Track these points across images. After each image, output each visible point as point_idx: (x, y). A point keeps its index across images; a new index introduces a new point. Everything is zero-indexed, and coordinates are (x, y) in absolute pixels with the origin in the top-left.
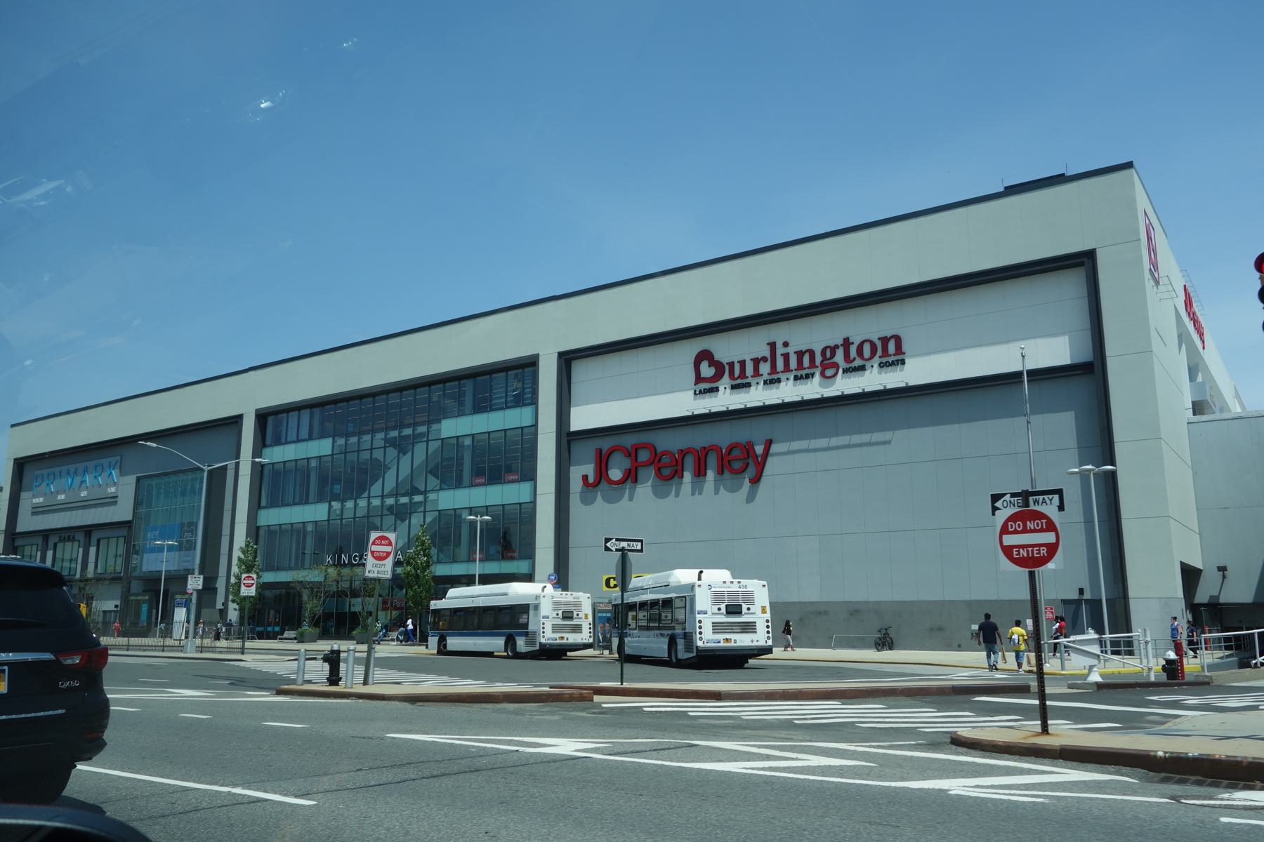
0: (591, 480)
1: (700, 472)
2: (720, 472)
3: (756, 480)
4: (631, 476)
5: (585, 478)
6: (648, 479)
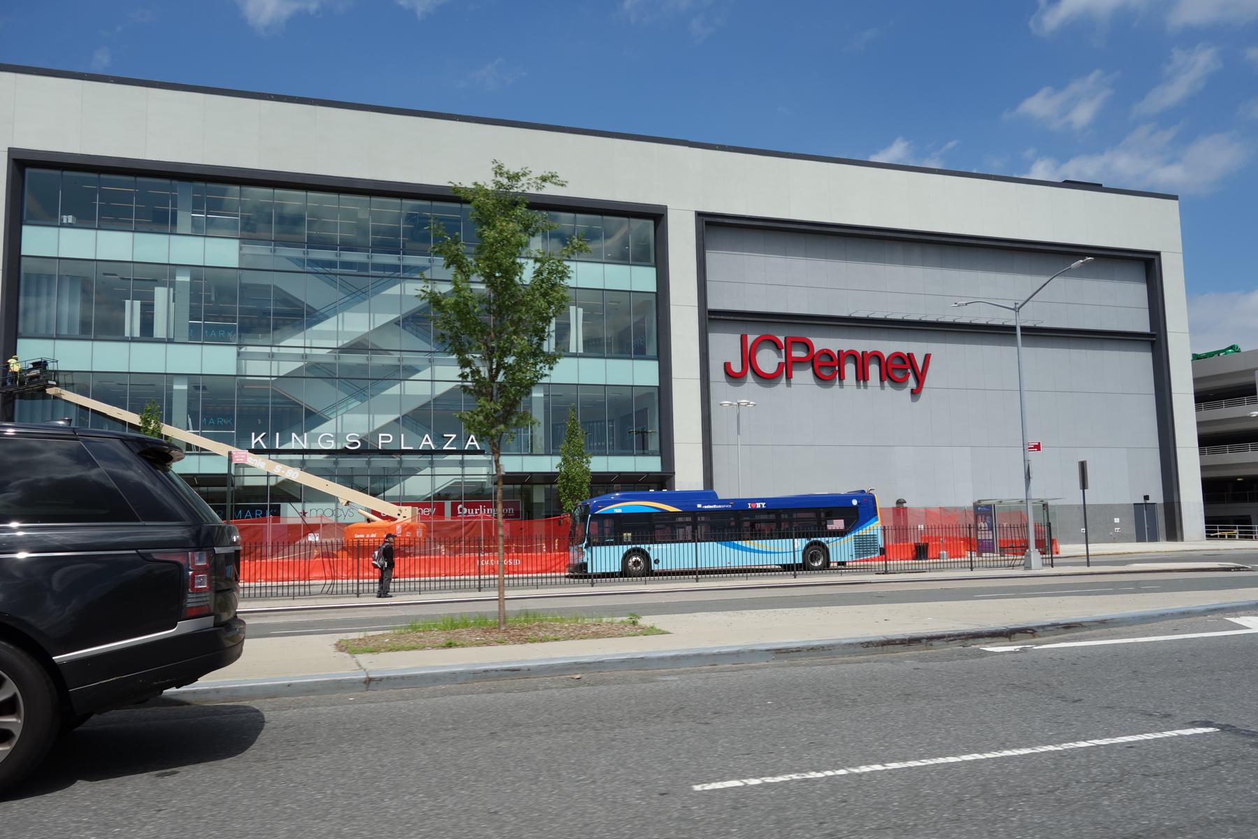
0: (736, 368)
1: (862, 376)
2: (882, 380)
3: (915, 393)
4: (786, 369)
5: (727, 366)
6: (804, 376)
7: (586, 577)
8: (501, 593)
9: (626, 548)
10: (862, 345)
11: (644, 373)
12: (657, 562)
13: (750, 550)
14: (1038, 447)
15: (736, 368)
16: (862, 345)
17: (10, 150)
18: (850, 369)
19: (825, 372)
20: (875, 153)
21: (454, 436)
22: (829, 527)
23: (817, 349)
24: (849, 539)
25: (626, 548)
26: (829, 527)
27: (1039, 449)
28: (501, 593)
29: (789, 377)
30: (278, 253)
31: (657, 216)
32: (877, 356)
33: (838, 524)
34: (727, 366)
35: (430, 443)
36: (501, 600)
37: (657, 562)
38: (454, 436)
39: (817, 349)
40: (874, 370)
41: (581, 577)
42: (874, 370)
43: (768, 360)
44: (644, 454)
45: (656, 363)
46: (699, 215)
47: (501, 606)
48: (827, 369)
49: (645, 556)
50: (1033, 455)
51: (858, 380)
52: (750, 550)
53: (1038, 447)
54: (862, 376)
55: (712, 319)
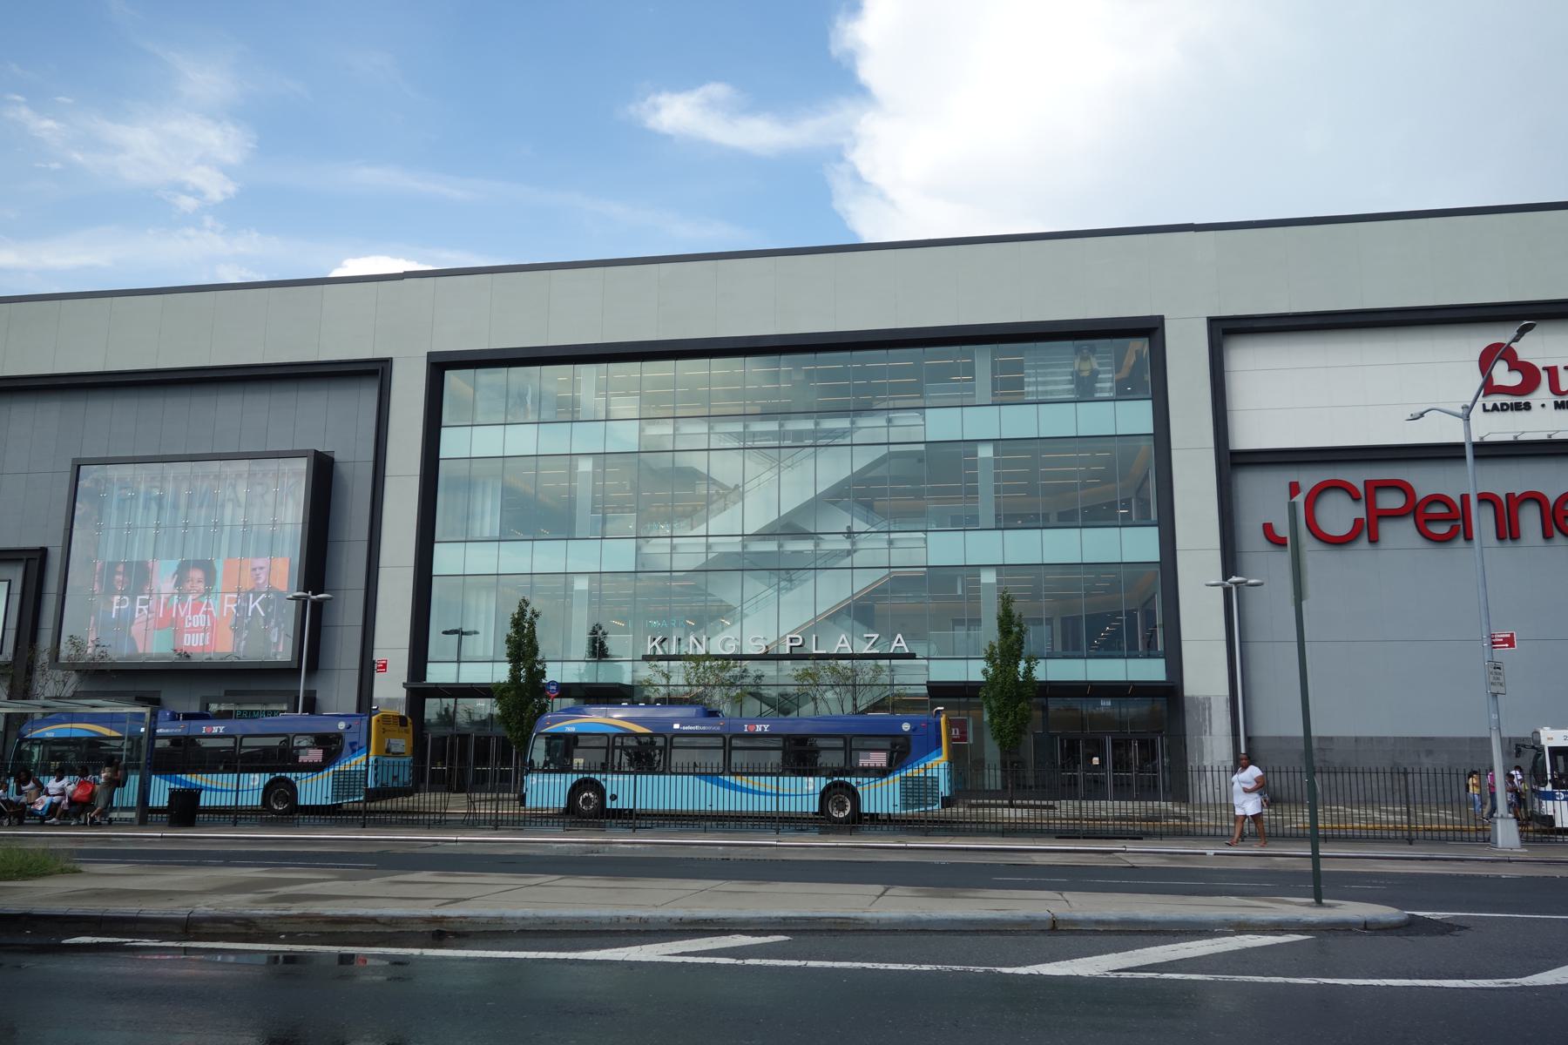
1: (1508, 530)
2: (1547, 535)
4: (1368, 529)
5: (1268, 529)
6: (1399, 534)
7: (1552, 832)
8: (1315, 849)
9: (575, 777)
10: (1507, 480)
11: (1141, 545)
12: (614, 797)
13: (741, 789)
14: (1510, 641)
15: (1282, 530)
16: (1507, 480)
17: (429, 354)
18: (1483, 521)
19: (1441, 529)
20: (339, 265)
21: (876, 636)
22: (863, 762)
23: (1421, 494)
24: (893, 783)
25: (572, 778)
26: (302, 759)
27: (1512, 645)
28: (1315, 849)
29: (1374, 539)
30: (896, 422)
31: (1150, 330)
32: (1536, 498)
33: (879, 759)
34: (1268, 529)
35: (903, 644)
36: (1316, 858)
37: (614, 797)
38: (876, 636)
39: (1421, 494)
40: (1530, 518)
41: (1545, 832)
42: (1530, 518)
43: (1338, 514)
44: (1149, 657)
45: (1155, 530)
46: (1212, 321)
47: (1316, 864)
48: (1443, 522)
49: (599, 790)
50: (1502, 653)
51: (1500, 537)
52: (741, 789)
53: (1510, 641)
54: (1508, 530)
55: (1233, 463)
